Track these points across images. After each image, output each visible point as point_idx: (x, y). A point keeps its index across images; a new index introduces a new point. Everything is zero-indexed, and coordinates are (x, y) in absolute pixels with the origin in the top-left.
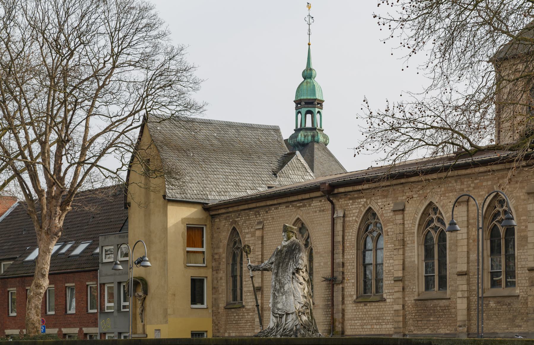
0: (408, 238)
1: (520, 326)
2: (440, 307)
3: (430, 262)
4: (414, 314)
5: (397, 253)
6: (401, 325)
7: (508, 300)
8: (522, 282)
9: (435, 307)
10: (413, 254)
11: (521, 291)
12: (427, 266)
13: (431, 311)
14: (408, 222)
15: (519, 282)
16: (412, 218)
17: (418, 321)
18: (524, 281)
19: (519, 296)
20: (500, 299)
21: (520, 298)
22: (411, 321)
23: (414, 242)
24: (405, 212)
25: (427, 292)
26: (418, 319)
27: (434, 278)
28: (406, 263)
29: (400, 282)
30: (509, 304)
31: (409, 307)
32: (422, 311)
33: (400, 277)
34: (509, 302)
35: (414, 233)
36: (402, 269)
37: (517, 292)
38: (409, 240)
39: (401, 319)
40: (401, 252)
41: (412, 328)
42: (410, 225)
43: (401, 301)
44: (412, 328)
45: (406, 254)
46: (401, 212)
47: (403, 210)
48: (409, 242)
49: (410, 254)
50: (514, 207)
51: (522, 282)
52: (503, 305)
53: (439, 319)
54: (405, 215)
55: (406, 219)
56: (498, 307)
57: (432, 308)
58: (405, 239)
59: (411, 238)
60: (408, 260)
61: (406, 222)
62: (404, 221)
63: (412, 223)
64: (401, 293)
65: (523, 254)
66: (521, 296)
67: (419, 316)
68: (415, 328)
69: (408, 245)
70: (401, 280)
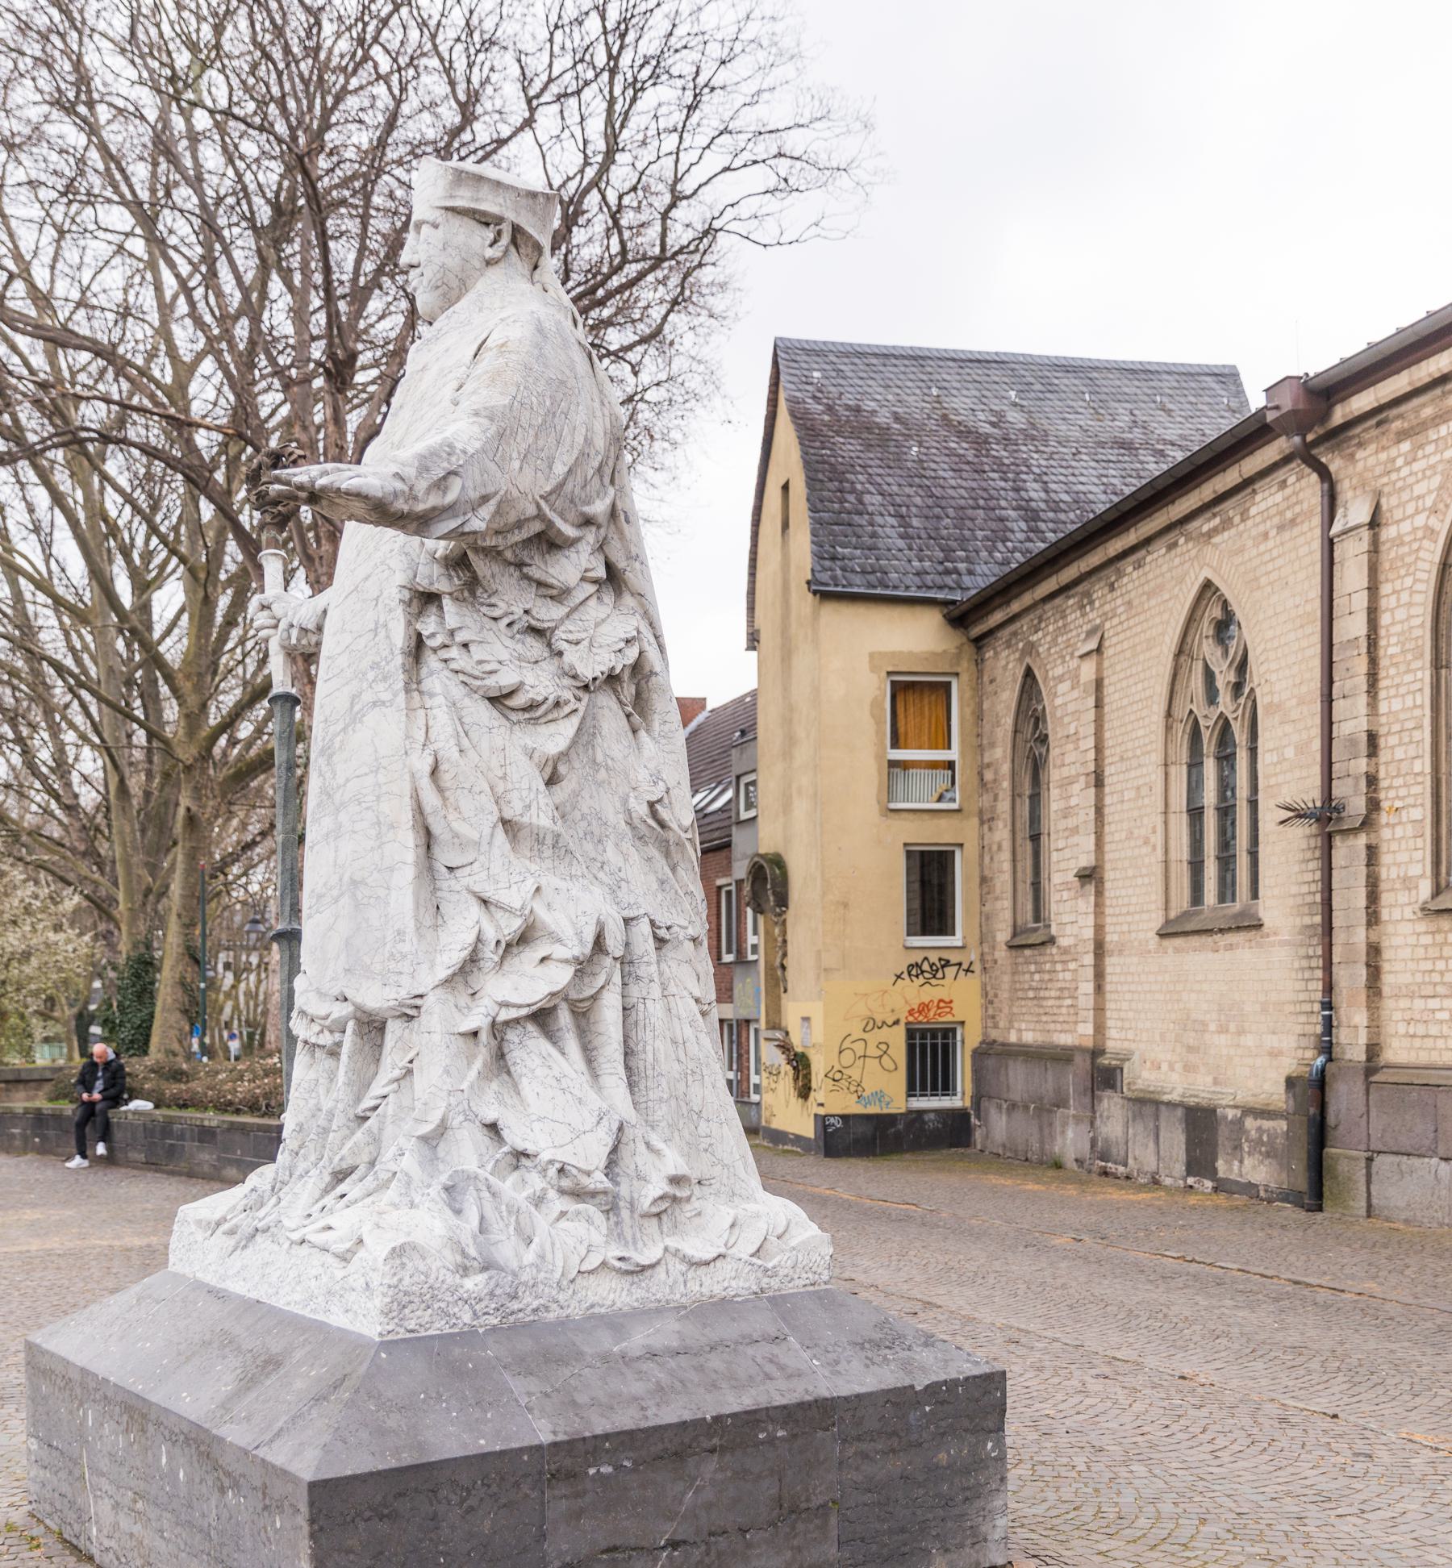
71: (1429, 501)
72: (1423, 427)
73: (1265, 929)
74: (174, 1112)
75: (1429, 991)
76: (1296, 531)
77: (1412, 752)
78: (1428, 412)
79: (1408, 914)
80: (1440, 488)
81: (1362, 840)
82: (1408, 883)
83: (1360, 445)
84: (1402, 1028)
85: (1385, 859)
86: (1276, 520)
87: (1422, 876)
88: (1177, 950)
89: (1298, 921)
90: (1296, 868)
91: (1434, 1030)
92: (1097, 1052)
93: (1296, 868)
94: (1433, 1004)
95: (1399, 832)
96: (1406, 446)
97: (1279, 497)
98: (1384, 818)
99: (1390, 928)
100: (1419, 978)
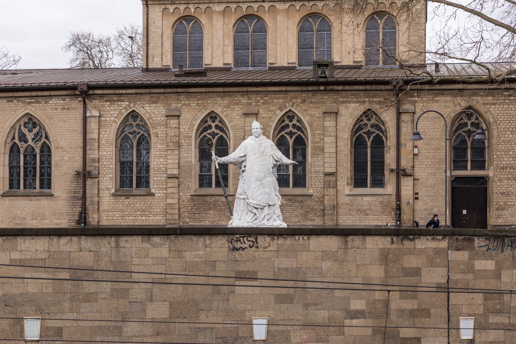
0: (183, 141)
1: (313, 220)
2: (223, 202)
3: (206, 163)
4: (190, 208)
5: (171, 154)
6: (177, 217)
7: (301, 199)
8: (316, 183)
9: (215, 202)
10: (190, 155)
11: (315, 191)
12: (202, 167)
13: (211, 206)
14: (184, 127)
15: (312, 184)
16: (189, 124)
17: (194, 214)
18: (319, 184)
19: (312, 195)
20: (291, 198)
21: (313, 197)
22: (186, 214)
23: (191, 145)
24: (180, 118)
25: (200, 189)
26: (195, 212)
27: (212, 177)
28: (181, 162)
29: (176, 179)
30: (302, 202)
31: (183, 201)
32: (200, 205)
33: (176, 174)
34: (301, 199)
35: (191, 136)
36: (177, 167)
37: (311, 192)
38: (185, 142)
39: (177, 211)
40: (176, 152)
41: (187, 220)
42: (187, 130)
43: (177, 196)
44: (187, 220)
45: (181, 155)
46: (176, 117)
47: (179, 116)
48: (185, 144)
49: (185, 155)
50: (308, 123)
51: (316, 183)
52: (295, 202)
53: (220, 212)
54: (181, 121)
55: (181, 124)
56: (289, 204)
57: (213, 203)
58: (180, 142)
59: (187, 141)
60: (184, 160)
61: (181, 127)
62: (179, 125)
63: (189, 128)
64: (177, 189)
65: (317, 161)
66: (314, 195)
67: (196, 209)
68: (191, 220)
69: (183, 147)
70: (177, 178)
71: (115, 116)
72: (114, 101)
73: (55, 196)
74: (498, 87)
75: (114, 210)
76: (69, 111)
77: (109, 163)
78: (115, 98)
79: (108, 195)
80: (118, 114)
81: (97, 180)
82: (107, 189)
83: (94, 99)
84: (105, 218)
85: (101, 184)
86: (61, 107)
87: (112, 188)
88: (10, 200)
89: (69, 195)
90: (69, 184)
91: (115, 218)
92: (236, 272)
93: (69, 184)
94: (116, 213)
95: (105, 179)
96: (108, 103)
97: (62, 102)
98: (100, 176)
99: (102, 198)
100: (110, 208)
